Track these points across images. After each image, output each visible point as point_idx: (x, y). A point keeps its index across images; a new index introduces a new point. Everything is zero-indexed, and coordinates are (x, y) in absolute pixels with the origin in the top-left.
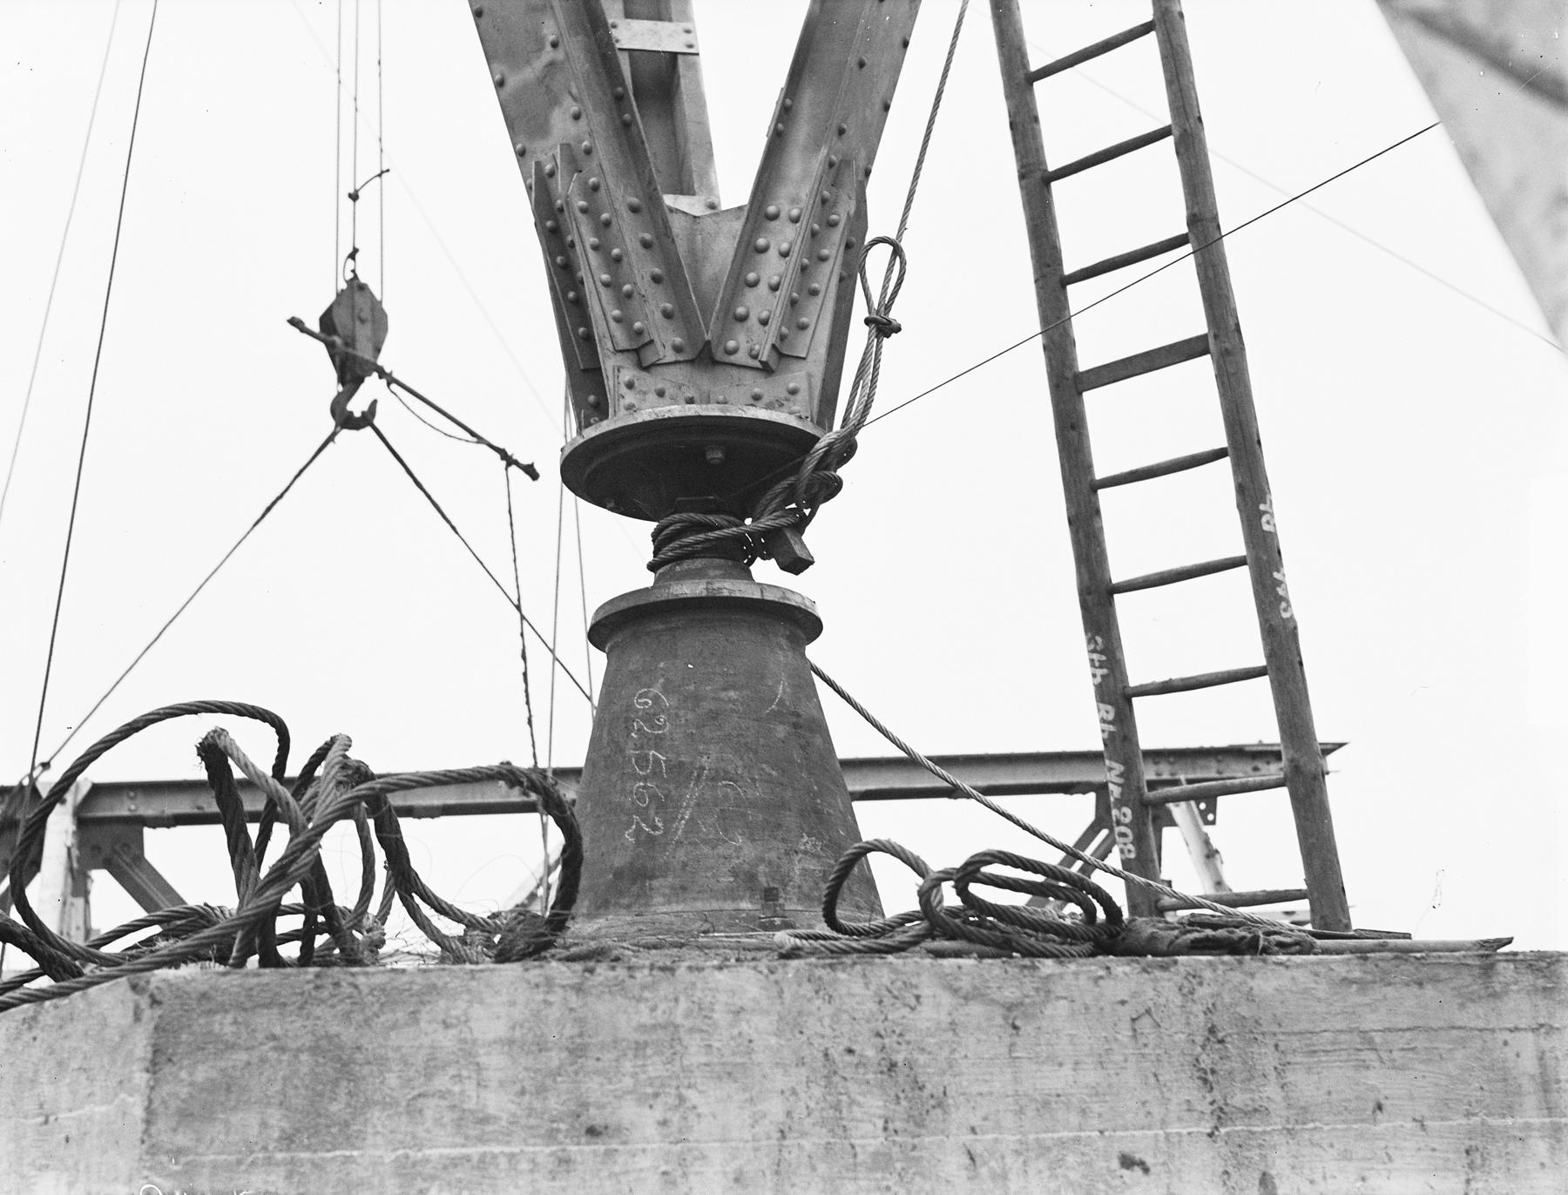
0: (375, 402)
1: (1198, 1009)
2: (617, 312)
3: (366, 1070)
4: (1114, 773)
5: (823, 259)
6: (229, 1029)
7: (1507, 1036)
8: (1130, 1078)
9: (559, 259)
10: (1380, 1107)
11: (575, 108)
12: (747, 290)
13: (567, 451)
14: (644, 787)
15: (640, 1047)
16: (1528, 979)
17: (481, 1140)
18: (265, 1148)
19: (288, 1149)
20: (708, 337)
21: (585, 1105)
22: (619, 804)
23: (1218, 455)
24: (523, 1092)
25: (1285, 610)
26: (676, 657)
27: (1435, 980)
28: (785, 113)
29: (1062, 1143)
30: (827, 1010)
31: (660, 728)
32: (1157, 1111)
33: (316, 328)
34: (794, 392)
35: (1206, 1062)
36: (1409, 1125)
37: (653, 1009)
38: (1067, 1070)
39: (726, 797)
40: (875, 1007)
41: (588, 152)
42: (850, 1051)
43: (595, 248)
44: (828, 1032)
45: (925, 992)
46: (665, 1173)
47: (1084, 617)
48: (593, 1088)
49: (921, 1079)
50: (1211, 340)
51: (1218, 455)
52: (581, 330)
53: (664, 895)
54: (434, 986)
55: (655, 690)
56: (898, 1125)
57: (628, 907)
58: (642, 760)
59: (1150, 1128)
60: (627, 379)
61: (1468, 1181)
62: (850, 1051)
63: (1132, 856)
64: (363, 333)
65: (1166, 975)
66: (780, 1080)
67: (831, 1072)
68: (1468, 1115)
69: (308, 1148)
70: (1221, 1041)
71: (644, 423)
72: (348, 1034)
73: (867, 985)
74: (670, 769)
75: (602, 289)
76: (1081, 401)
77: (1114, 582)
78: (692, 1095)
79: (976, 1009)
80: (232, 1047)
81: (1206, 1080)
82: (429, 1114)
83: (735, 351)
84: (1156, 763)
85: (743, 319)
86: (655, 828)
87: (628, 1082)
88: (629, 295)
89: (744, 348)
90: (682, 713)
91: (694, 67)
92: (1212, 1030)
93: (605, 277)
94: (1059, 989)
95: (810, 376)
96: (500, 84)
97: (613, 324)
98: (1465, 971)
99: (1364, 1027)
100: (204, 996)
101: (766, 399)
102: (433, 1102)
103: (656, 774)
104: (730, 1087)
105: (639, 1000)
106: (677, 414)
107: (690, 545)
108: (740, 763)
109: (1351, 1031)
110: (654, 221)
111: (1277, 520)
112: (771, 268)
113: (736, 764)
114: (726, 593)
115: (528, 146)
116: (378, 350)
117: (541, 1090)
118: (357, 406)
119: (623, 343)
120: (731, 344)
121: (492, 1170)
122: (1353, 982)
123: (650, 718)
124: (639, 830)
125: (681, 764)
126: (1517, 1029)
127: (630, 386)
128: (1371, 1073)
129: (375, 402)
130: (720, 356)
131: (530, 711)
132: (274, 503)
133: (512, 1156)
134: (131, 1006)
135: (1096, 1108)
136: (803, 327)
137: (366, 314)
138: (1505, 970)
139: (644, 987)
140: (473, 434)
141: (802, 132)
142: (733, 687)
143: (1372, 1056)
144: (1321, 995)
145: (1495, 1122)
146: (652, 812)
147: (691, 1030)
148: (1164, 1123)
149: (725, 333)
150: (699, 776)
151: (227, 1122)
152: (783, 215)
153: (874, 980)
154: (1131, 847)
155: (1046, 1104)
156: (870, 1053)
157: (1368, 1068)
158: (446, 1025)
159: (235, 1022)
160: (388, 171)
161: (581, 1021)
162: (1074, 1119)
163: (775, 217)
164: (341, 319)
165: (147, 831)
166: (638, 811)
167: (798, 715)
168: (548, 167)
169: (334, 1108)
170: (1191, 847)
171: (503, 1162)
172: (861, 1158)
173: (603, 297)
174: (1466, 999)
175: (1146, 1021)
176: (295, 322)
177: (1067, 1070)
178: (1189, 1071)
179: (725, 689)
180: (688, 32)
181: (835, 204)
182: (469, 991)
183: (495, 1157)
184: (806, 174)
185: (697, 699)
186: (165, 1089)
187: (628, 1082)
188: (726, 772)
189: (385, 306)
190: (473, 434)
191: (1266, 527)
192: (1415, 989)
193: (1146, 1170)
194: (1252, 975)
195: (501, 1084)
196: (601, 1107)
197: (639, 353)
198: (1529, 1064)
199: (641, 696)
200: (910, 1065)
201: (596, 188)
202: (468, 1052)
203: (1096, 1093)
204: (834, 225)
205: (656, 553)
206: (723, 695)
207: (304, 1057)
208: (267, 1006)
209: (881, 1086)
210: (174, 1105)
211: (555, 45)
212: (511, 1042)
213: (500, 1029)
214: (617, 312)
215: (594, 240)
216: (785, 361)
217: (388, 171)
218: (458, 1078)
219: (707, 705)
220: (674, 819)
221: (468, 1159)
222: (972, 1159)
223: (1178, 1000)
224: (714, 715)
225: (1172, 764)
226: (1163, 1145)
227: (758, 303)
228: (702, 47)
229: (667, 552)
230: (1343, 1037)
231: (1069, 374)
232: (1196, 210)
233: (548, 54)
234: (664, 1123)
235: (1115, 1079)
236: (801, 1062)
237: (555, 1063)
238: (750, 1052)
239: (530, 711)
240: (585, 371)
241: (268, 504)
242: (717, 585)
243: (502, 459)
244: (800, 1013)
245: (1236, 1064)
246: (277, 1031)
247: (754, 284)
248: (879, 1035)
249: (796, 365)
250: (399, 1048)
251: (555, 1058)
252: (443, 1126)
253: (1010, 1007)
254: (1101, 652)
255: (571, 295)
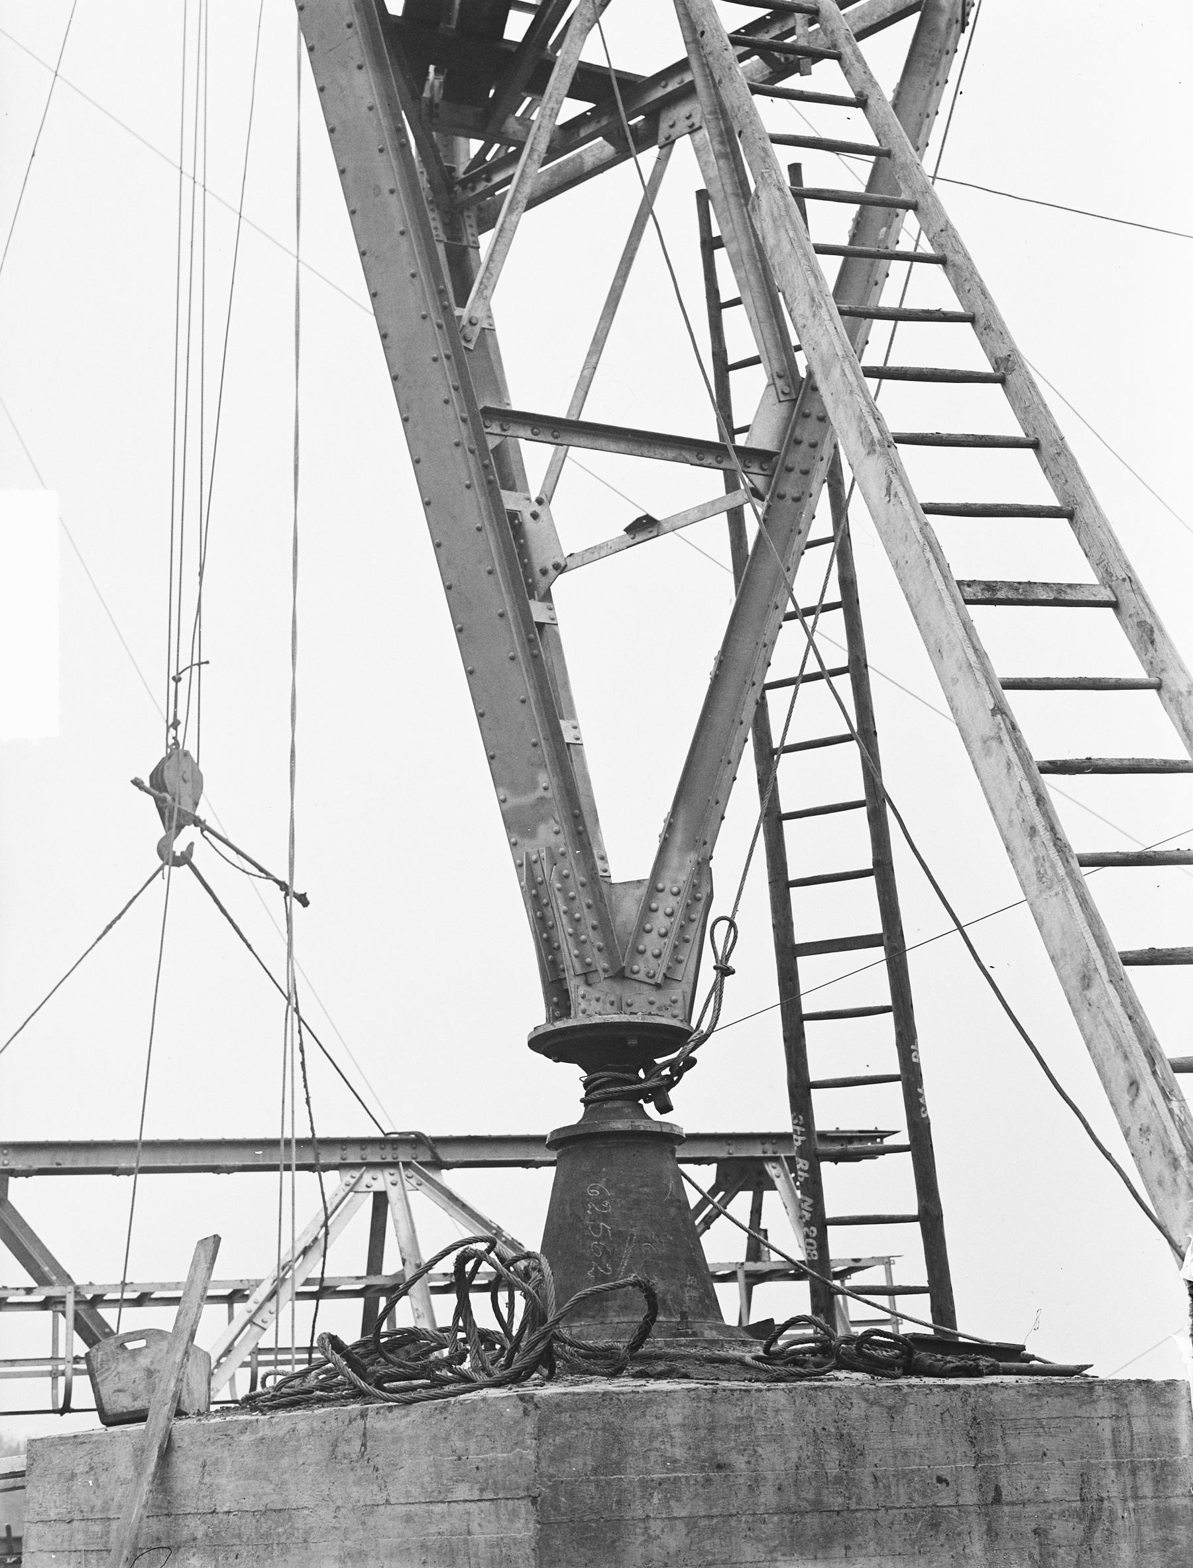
0: (192, 844)
1: (968, 1408)
2: (576, 952)
3: (625, 1438)
4: (806, 1204)
5: (693, 921)
6: (568, 1420)
7: (1099, 1421)
8: (941, 1441)
9: (538, 913)
10: (1045, 1454)
11: (556, 828)
12: (645, 934)
13: (541, 1031)
14: (598, 1245)
15: (737, 1427)
16: (1108, 1394)
17: (674, 1471)
18: (586, 1475)
19: (595, 1475)
20: (624, 965)
21: (716, 1454)
22: (582, 1254)
23: (884, 1010)
24: (690, 1448)
25: (924, 1112)
26: (612, 1165)
27: (1068, 1394)
28: (670, 827)
29: (912, 1471)
30: (814, 1410)
31: (605, 1209)
32: (952, 1458)
33: (147, 784)
34: (675, 1002)
35: (972, 1433)
36: (1057, 1463)
37: (742, 1410)
38: (914, 1438)
39: (647, 1251)
40: (833, 1408)
41: (563, 854)
42: (824, 1429)
43: (565, 912)
44: (814, 1420)
45: (854, 1401)
46: (750, 1486)
47: (791, 1102)
48: (718, 1446)
49: (854, 1441)
50: (885, 938)
51: (884, 1010)
52: (550, 957)
53: (615, 1311)
54: (651, 1399)
55: (601, 1185)
56: (845, 1463)
57: (594, 1317)
58: (596, 1228)
59: (949, 1464)
60: (582, 993)
61: (1081, 1489)
62: (824, 1429)
63: (816, 1258)
64: (186, 790)
65: (955, 1393)
66: (795, 1443)
67: (817, 1439)
68: (1082, 1458)
69: (603, 1475)
70: (979, 1424)
71: (596, 1024)
72: (617, 1422)
73: (830, 1398)
74: (613, 1235)
75: (568, 937)
76: (796, 963)
77: (811, 1080)
78: (759, 1449)
79: (876, 1408)
80: (570, 1428)
81: (972, 1441)
82: (652, 1459)
83: (637, 972)
84: (763, 1144)
85: (643, 953)
86: (607, 1270)
87: (733, 1443)
88: (584, 942)
89: (643, 971)
90: (618, 1200)
91: (580, 754)
92: (975, 1419)
93: (570, 930)
94: (910, 1400)
95: (684, 992)
96: (502, 802)
97: (574, 959)
98: (1082, 1391)
99: (1038, 1417)
100: (557, 1405)
101: (657, 1005)
102: (653, 1453)
103: (604, 1237)
104: (775, 1446)
105: (736, 1405)
106: (617, 1020)
107: (612, 1093)
108: (653, 1233)
109: (1033, 1418)
110: (594, 893)
111: (920, 1055)
112: (660, 922)
113: (651, 1234)
114: (642, 1129)
115: (519, 841)
116: (196, 804)
117: (698, 1448)
118: (179, 847)
119: (579, 971)
120: (636, 968)
121: (679, 1484)
122: (1035, 1395)
123: (599, 1202)
124: (596, 1271)
125: (621, 1232)
126: (1103, 1417)
127: (583, 997)
128: (1041, 1438)
129: (192, 844)
130: (628, 973)
131: (307, 1093)
132: (114, 922)
133: (687, 1478)
134: (522, 1408)
135: (927, 1455)
136: (680, 962)
137: (188, 776)
138: (1099, 1389)
139: (738, 1400)
140: (261, 870)
141: (678, 838)
142: (647, 1186)
143: (1041, 1430)
144: (1020, 1401)
145: (1092, 1461)
146: (604, 1260)
147: (758, 1420)
148: (955, 1462)
149: (632, 961)
150: (631, 1240)
151: (570, 1462)
152: (667, 889)
153: (834, 1396)
154: (815, 1252)
155: (906, 1453)
156: (833, 1430)
157: (1040, 1436)
158: (657, 1418)
159: (570, 1416)
160: (207, 662)
161: (711, 1415)
162: (917, 1460)
163: (662, 891)
164: (169, 776)
165: (11, 1179)
166: (596, 1259)
167: (680, 1201)
168: (534, 857)
169: (614, 1455)
170: (789, 1209)
171: (683, 1480)
172: (830, 1478)
173: (570, 943)
174: (1082, 1403)
175: (947, 1413)
176: (137, 783)
177: (914, 1438)
178: (965, 1437)
179: (643, 1187)
180: (575, 728)
181: (699, 887)
182: (666, 1402)
183: (680, 1478)
184: (681, 867)
185: (626, 1192)
186: (544, 1447)
187: (733, 1443)
188: (647, 1238)
189: (202, 768)
190: (261, 870)
191: (914, 1060)
192: (1060, 1399)
193: (948, 1484)
194: (992, 1393)
195: (681, 1444)
196: (722, 1455)
197: (587, 976)
198: (1108, 1434)
199: (591, 1188)
200: (849, 1435)
201: (567, 876)
202: (666, 1429)
203: (927, 1449)
204: (699, 900)
205: (586, 1095)
206: (641, 1189)
207: (600, 1433)
208: (583, 1409)
209: (837, 1445)
210: (547, 1454)
211: (546, 789)
212: (684, 1425)
213: (679, 1419)
214: (576, 952)
215: (564, 908)
216: (668, 982)
217: (207, 662)
218: (663, 1442)
219: (634, 1196)
220: (618, 1266)
221: (669, 1479)
222: (876, 1479)
223: (960, 1405)
224: (637, 1202)
225: (773, 1144)
226: (954, 1472)
227: (651, 943)
228: (585, 740)
229: (596, 1095)
230: (1030, 1421)
231: (789, 945)
232: (880, 858)
233: (540, 793)
234: (749, 1462)
235: (934, 1442)
236: (804, 1434)
237: (703, 1435)
238: (783, 1429)
239: (307, 1093)
240: (553, 982)
241: (109, 922)
242: (637, 1124)
243: (282, 889)
244: (803, 1412)
245: (985, 1435)
246: (588, 1420)
247: (649, 932)
248: (836, 1421)
249: (675, 984)
250: (638, 1429)
251: (703, 1433)
252: (658, 1464)
253: (890, 1408)
254: (802, 1126)
255: (545, 935)
